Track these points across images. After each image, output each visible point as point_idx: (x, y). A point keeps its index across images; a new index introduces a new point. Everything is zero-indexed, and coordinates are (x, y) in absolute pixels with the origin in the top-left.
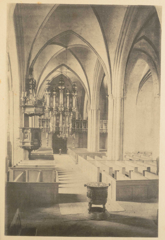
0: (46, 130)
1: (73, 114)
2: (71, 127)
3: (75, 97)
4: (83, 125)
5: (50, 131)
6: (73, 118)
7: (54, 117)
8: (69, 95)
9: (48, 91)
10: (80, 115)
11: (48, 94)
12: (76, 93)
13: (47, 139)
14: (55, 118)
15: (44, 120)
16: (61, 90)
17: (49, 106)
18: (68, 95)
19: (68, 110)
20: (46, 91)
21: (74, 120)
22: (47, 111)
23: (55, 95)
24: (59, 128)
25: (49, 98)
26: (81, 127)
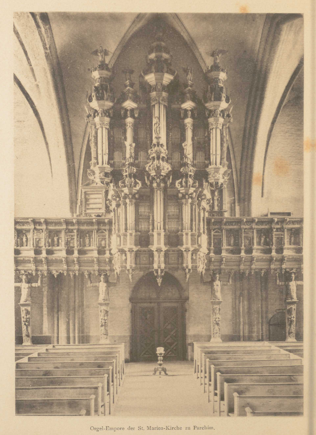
0: (99, 271)
1: (213, 193)
2: (204, 249)
3: (221, 120)
4: (259, 244)
5: (112, 270)
6: (211, 212)
7: (125, 204)
8: (192, 111)
9: (100, 98)
10: (237, 208)
11: (130, 196)
12: (223, 99)
13: (104, 308)
14: (131, 209)
15: (84, 227)
16: (155, 89)
17: (109, 163)
18: (186, 110)
19: (191, 170)
20: (91, 100)
21: (214, 223)
22: (100, 184)
23: (132, 116)
24: (151, 254)
25: (105, 133)
26: (249, 251)
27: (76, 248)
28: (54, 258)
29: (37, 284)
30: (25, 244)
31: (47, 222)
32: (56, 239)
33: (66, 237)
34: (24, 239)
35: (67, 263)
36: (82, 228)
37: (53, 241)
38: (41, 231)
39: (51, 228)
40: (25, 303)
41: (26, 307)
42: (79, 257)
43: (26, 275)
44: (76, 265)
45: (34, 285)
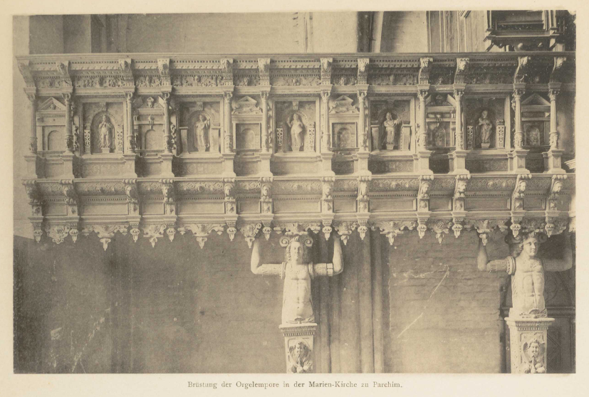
0: (524, 222)
27: (361, 150)
28: (394, 184)
29: (330, 265)
30: (201, 142)
31: (274, 71)
32: (390, 126)
33: (136, 123)
34: (296, 130)
35: (431, 201)
36: (382, 89)
37: (383, 134)
38: (350, 100)
39: (382, 89)
40: (298, 325)
41: (300, 339)
42: (138, 184)
43: (301, 239)
44: (361, 205)
45: (322, 268)
